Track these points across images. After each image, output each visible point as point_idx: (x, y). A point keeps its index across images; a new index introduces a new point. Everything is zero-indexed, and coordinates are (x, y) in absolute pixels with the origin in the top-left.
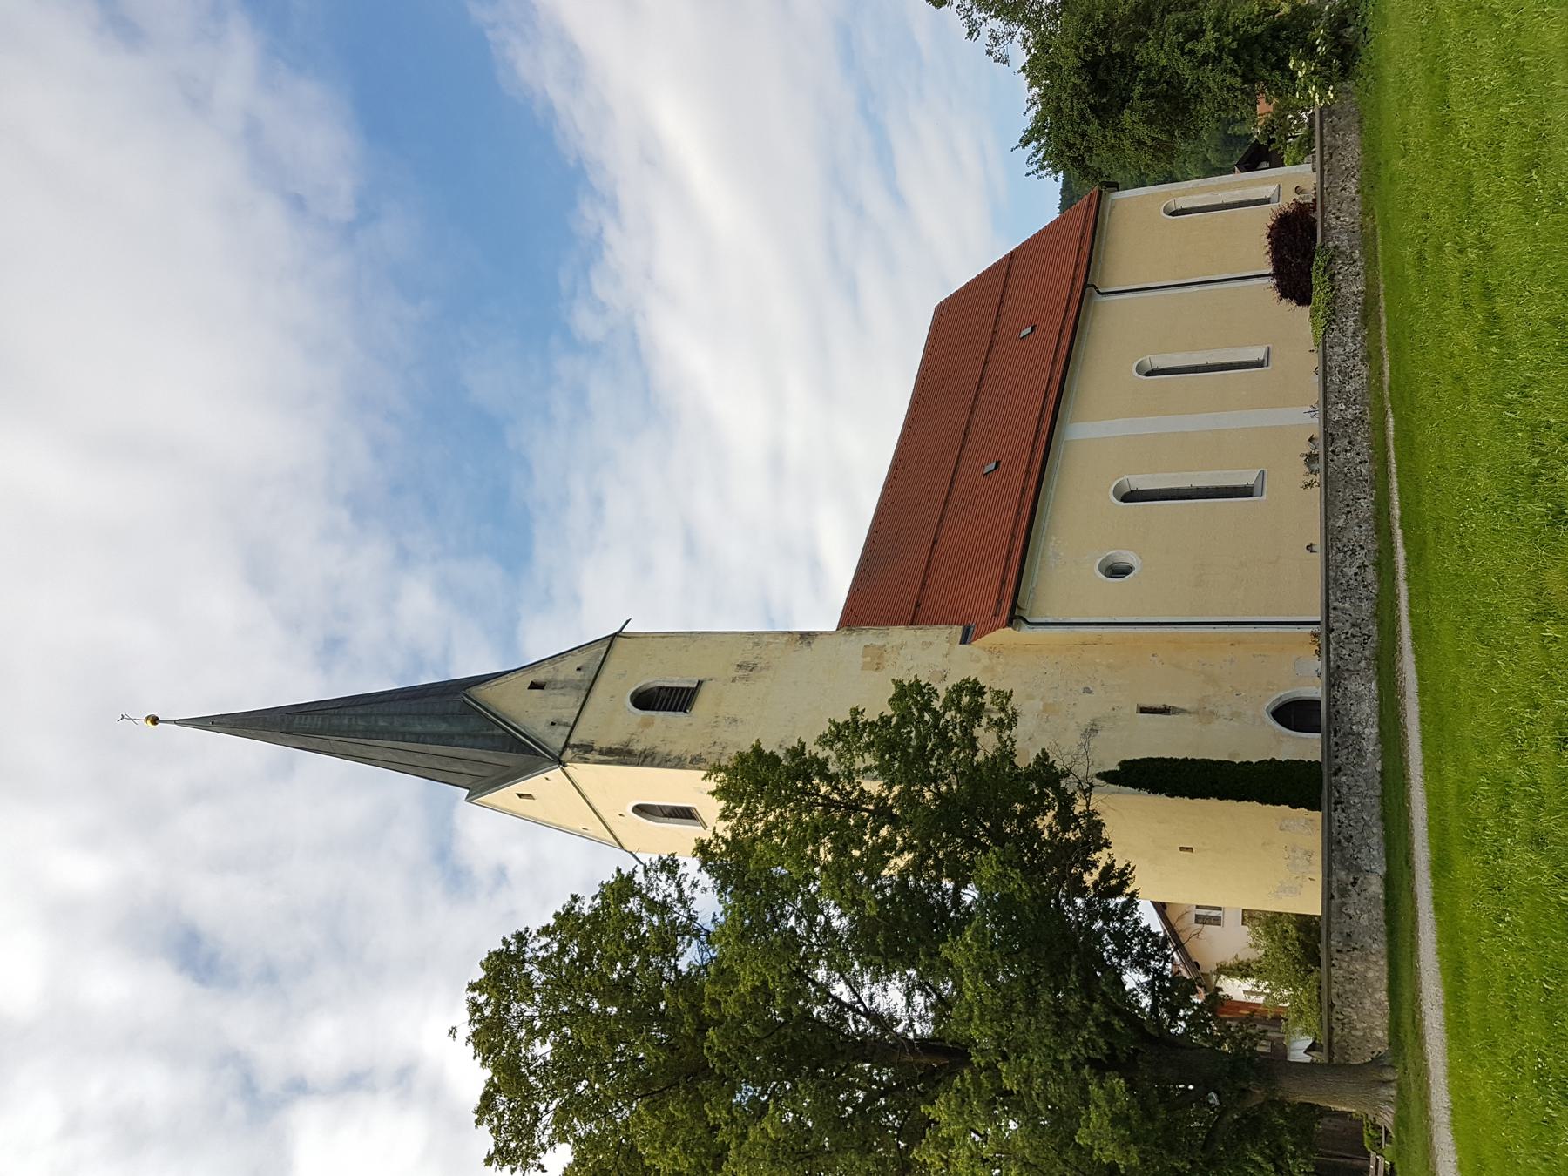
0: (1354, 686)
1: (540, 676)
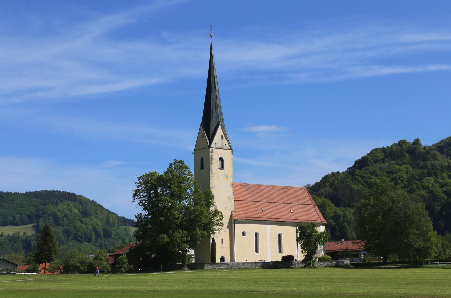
0: (226, 266)
1: (224, 137)
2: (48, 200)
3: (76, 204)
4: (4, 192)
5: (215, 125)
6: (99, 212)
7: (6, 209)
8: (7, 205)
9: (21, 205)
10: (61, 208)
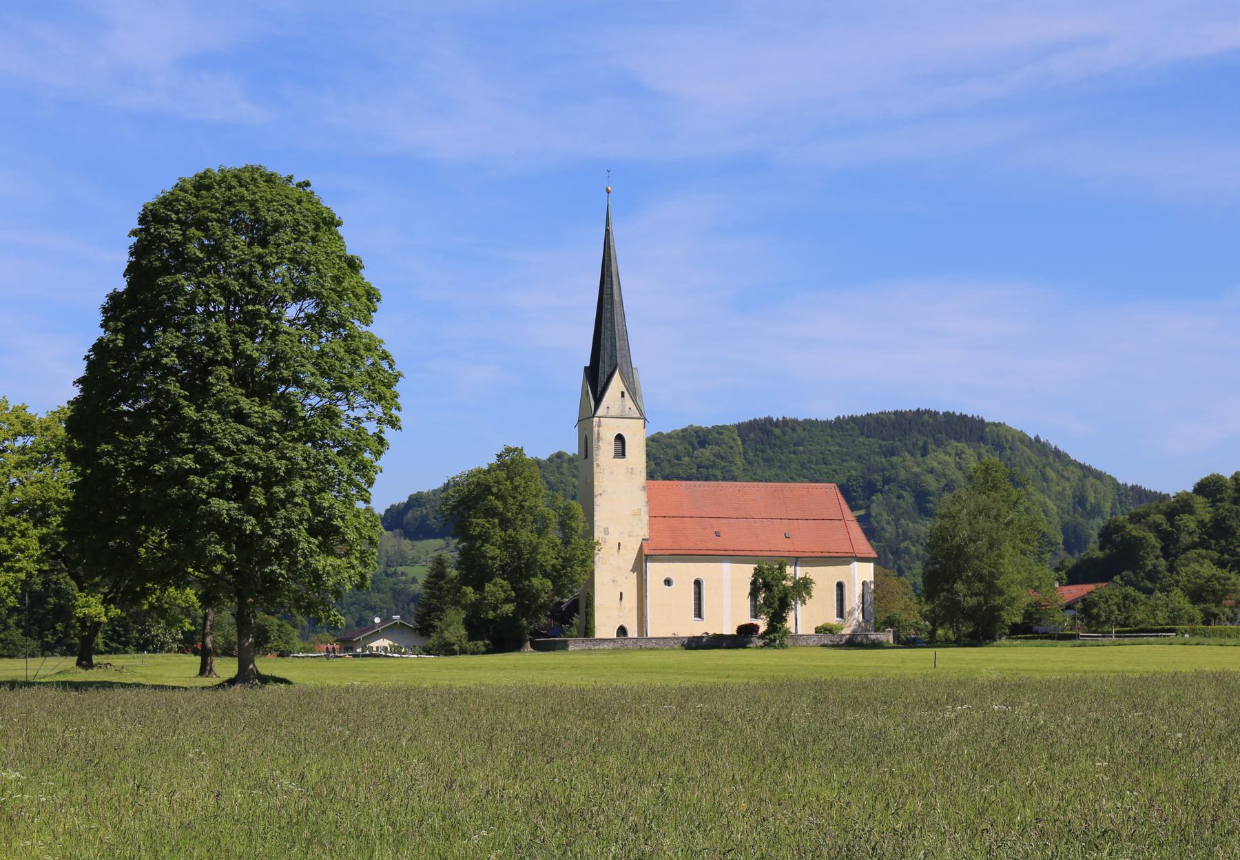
1: (626, 394)
2: (900, 441)
3: (983, 451)
4: (775, 420)
5: (608, 370)
6: (1052, 474)
7: (780, 467)
8: (782, 457)
9: (821, 456)
10: (935, 464)
